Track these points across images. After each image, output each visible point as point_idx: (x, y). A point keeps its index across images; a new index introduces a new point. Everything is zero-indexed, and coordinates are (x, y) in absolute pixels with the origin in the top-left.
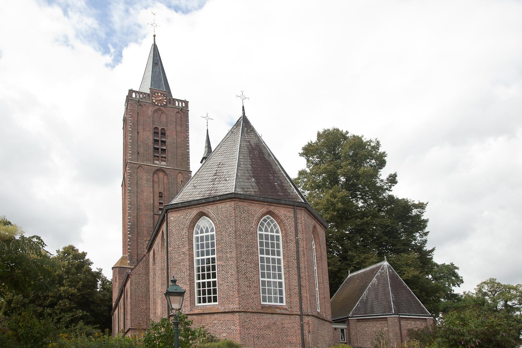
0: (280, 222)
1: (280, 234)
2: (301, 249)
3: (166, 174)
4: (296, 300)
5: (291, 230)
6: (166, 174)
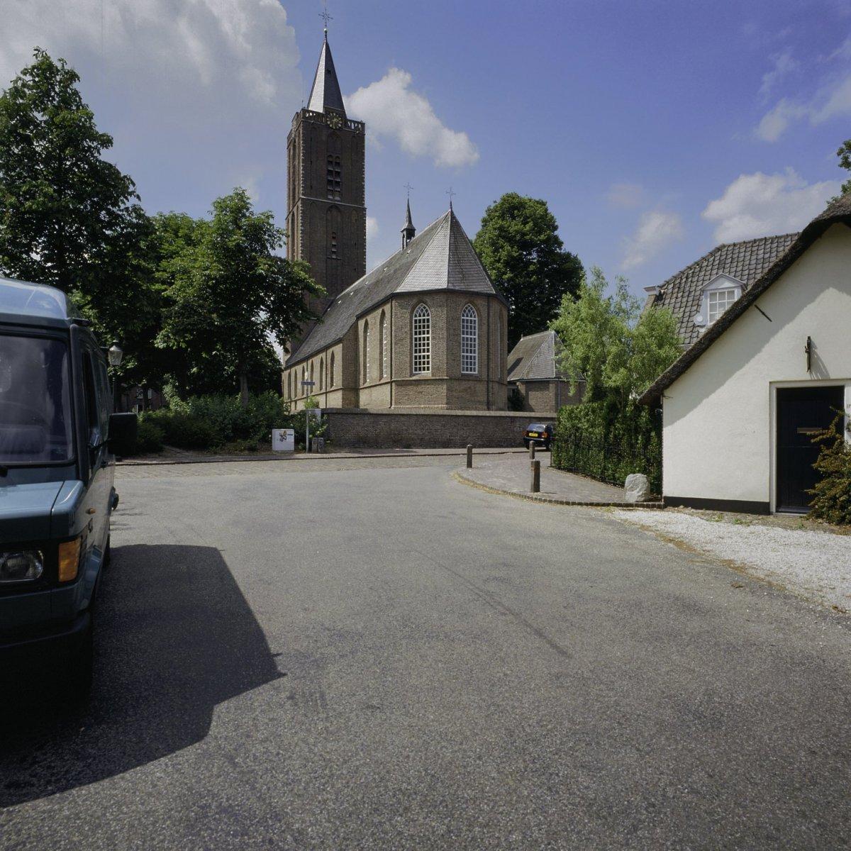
0: (478, 310)
1: (476, 319)
2: (491, 330)
3: (340, 211)
4: (485, 370)
5: (485, 315)
6: (340, 211)
